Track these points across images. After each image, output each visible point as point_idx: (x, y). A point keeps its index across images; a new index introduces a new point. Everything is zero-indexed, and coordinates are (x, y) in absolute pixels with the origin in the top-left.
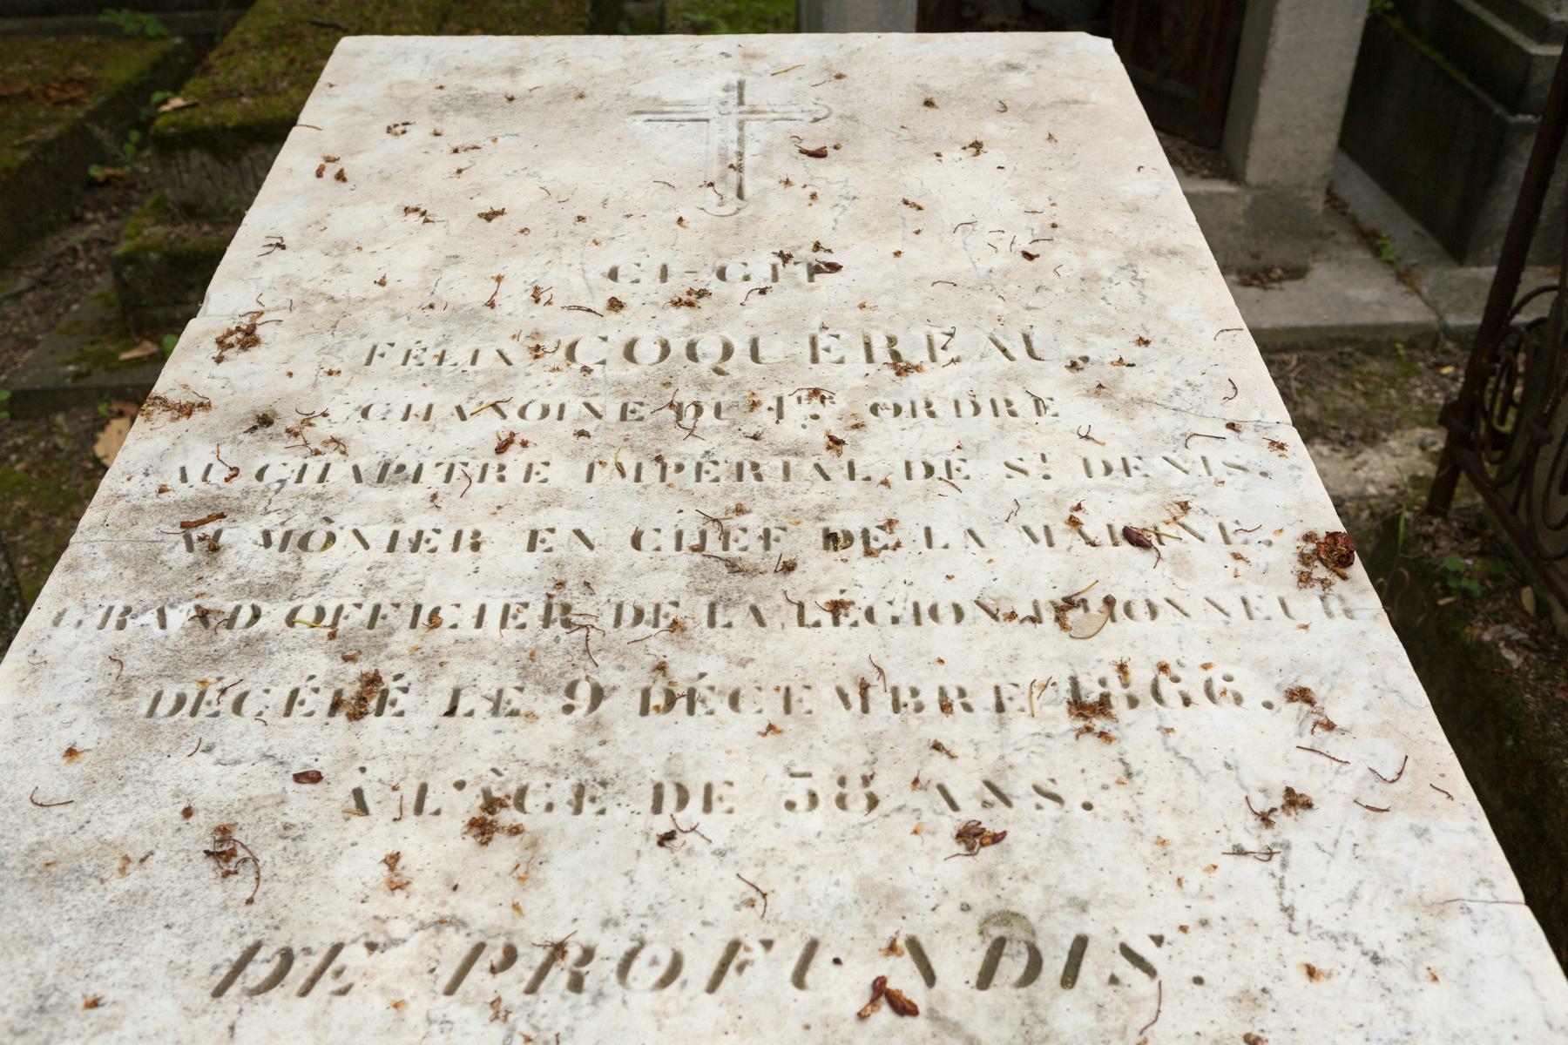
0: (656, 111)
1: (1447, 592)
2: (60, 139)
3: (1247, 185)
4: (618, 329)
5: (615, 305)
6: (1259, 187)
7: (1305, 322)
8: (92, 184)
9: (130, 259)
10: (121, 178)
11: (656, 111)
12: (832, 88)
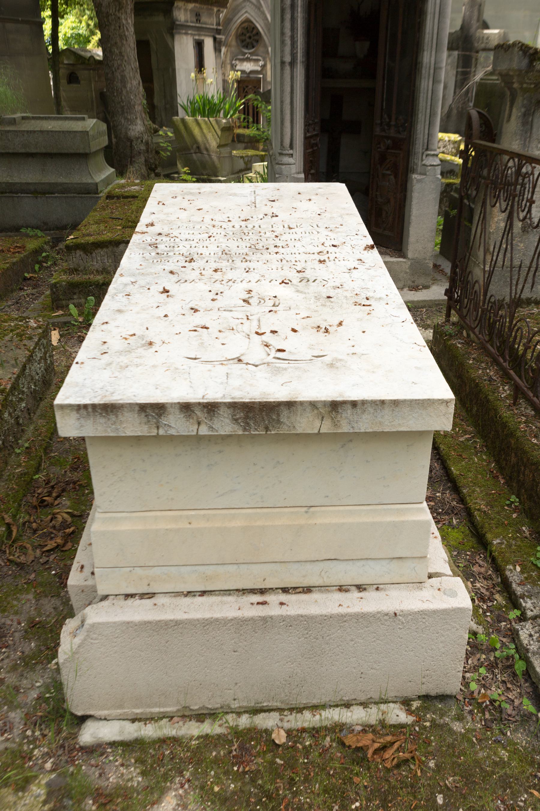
0: (235, 195)
1: (446, 336)
2: (17, 262)
3: (409, 259)
4: (230, 224)
5: (229, 221)
6: (412, 259)
7: (428, 299)
8: (25, 279)
9: (55, 285)
10: (35, 278)
11: (235, 195)
12: (277, 191)
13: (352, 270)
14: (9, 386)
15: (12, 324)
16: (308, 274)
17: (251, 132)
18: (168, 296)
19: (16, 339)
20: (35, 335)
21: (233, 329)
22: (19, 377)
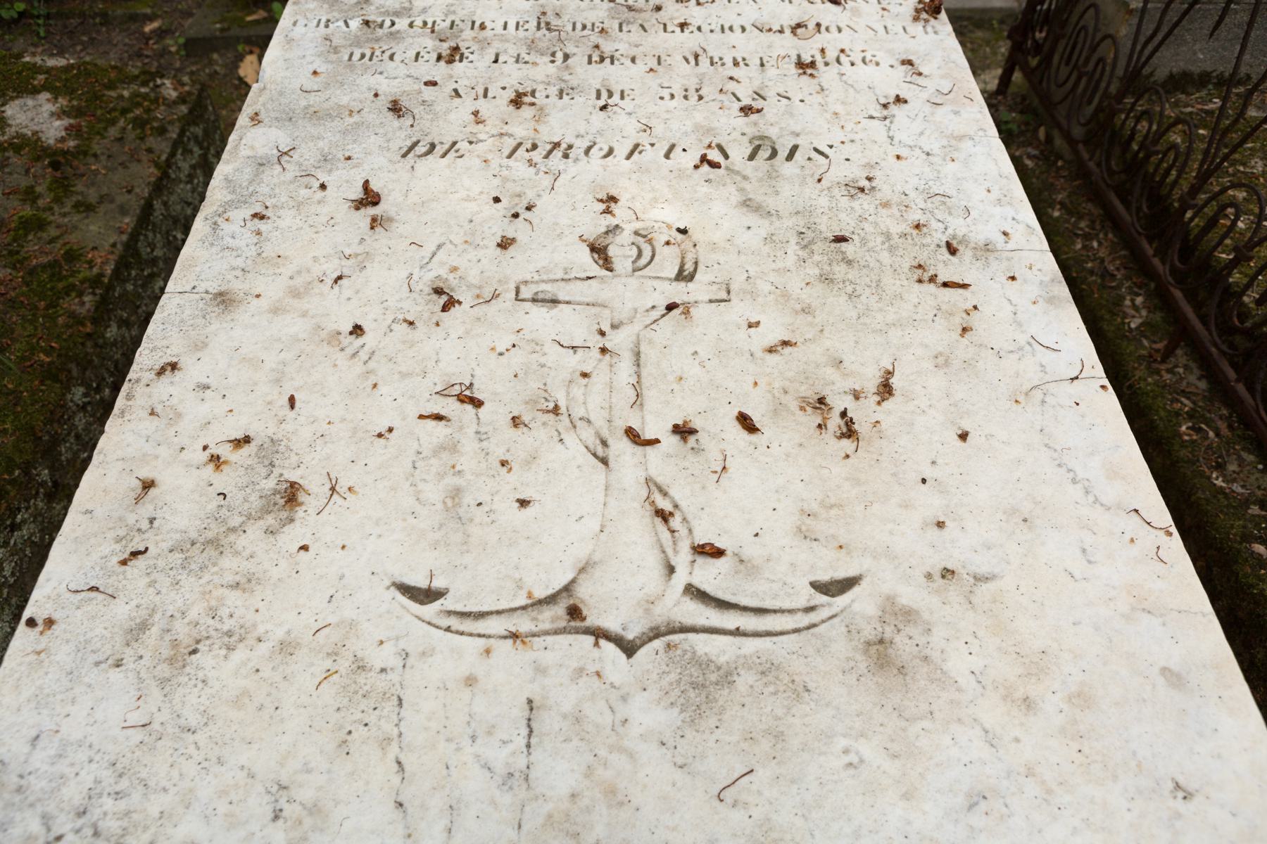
13: (894, 109)
14: (109, 270)
15: (126, 93)
16: (774, 122)
17: (806, 240)
18: (375, 222)
19: (131, 135)
20: (171, 122)
21: (556, 410)
22: (134, 237)
